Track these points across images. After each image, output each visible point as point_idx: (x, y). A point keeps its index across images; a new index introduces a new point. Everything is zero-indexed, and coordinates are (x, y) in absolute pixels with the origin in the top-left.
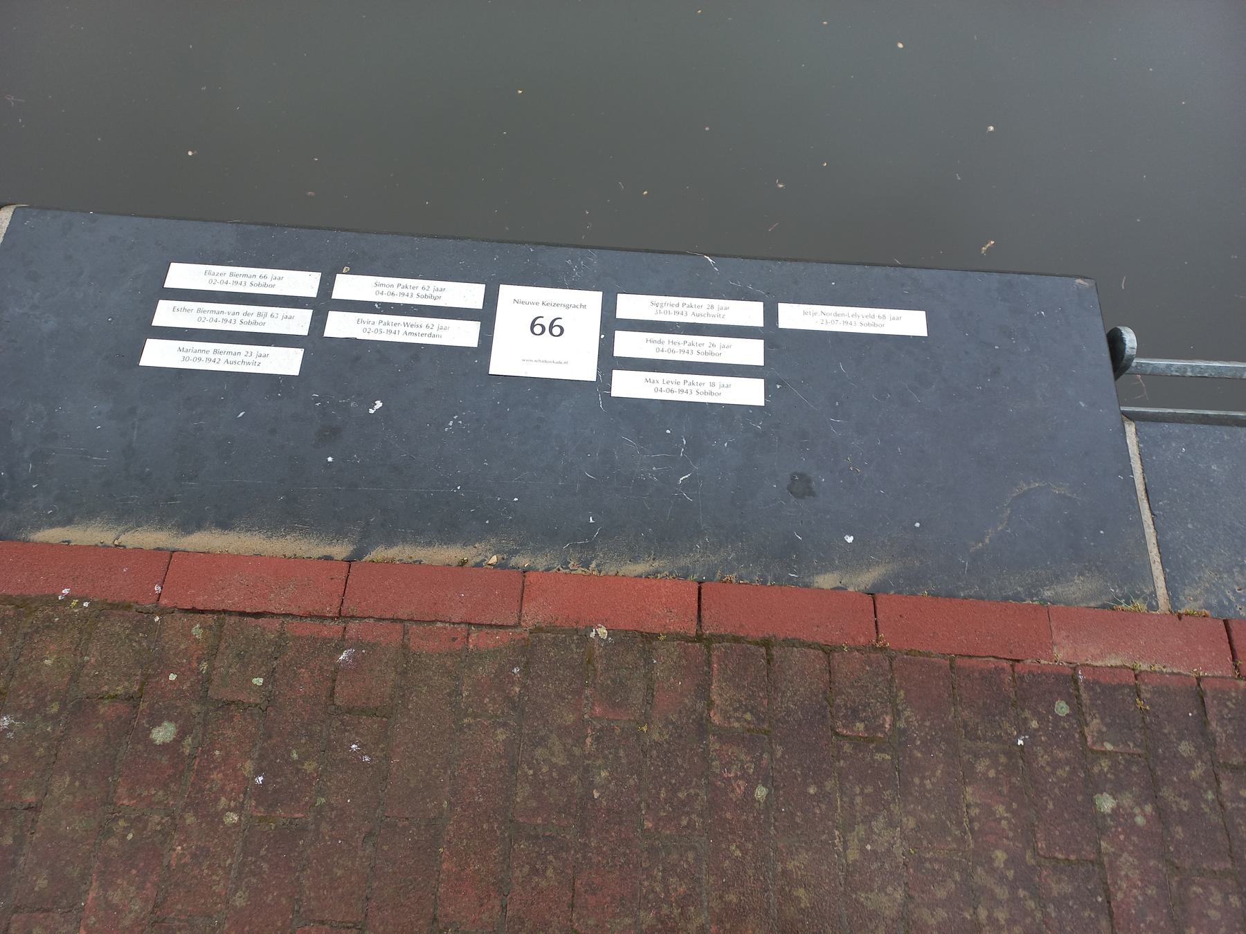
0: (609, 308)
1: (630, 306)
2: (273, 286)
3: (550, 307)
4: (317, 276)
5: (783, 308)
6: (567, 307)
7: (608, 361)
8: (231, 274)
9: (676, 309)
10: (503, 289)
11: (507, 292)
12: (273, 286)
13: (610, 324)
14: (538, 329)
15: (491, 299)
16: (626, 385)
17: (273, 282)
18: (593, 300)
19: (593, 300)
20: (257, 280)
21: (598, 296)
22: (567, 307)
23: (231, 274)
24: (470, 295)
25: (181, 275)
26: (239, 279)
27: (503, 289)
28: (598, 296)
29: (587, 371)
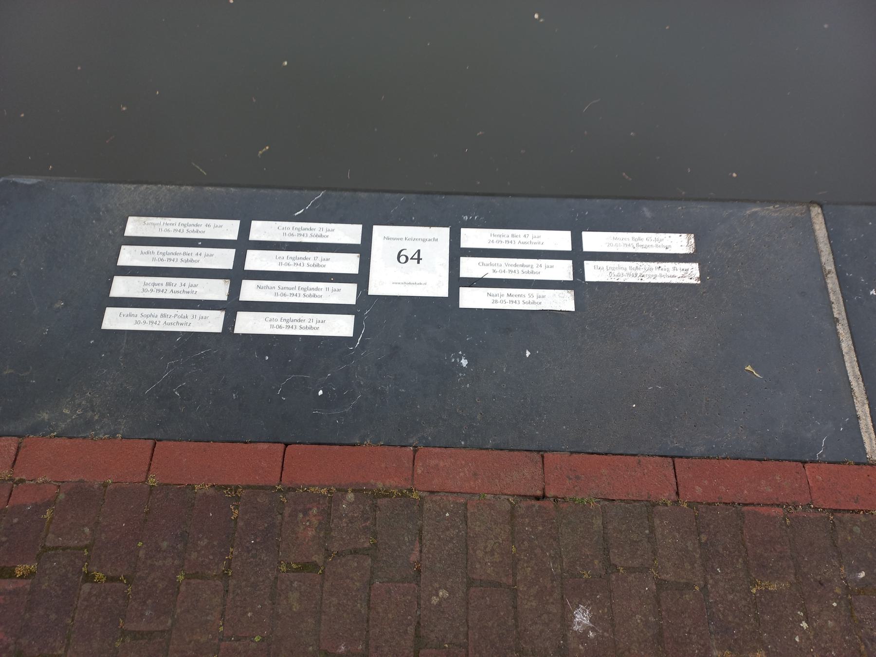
0: (455, 239)
1: (471, 237)
2: (324, 266)
3: (411, 242)
4: (359, 227)
5: (465, 232)
6: (424, 240)
7: (456, 282)
8: (509, 295)
9: (507, 239)
10: (376, 228)
11: (378, 231)
12: (324, 266)
13: (457, 252)
14: (403, 259)
15: (367, 236)
16: (470, 299)
17: (327, 234)
18: (444, 233)
19: (444, 233)
20: (527, 299)
21: (447, 230)
22: (424, 240)
23: (509, 295)
24: (351, 233)
25: (135, 227)
26: (514, 299)
27: (376, 228)
28: (447, 230)
29: (442, 290)
